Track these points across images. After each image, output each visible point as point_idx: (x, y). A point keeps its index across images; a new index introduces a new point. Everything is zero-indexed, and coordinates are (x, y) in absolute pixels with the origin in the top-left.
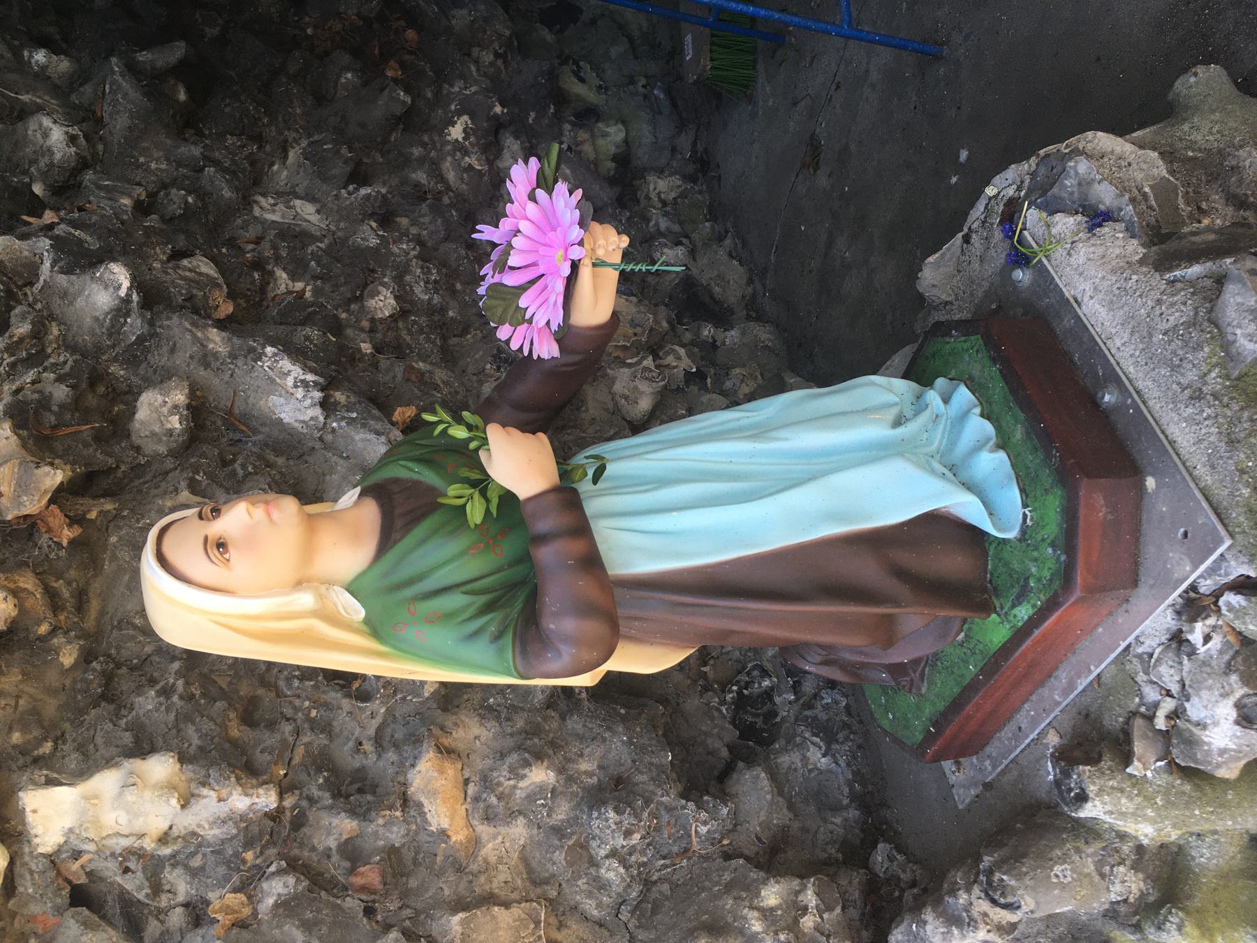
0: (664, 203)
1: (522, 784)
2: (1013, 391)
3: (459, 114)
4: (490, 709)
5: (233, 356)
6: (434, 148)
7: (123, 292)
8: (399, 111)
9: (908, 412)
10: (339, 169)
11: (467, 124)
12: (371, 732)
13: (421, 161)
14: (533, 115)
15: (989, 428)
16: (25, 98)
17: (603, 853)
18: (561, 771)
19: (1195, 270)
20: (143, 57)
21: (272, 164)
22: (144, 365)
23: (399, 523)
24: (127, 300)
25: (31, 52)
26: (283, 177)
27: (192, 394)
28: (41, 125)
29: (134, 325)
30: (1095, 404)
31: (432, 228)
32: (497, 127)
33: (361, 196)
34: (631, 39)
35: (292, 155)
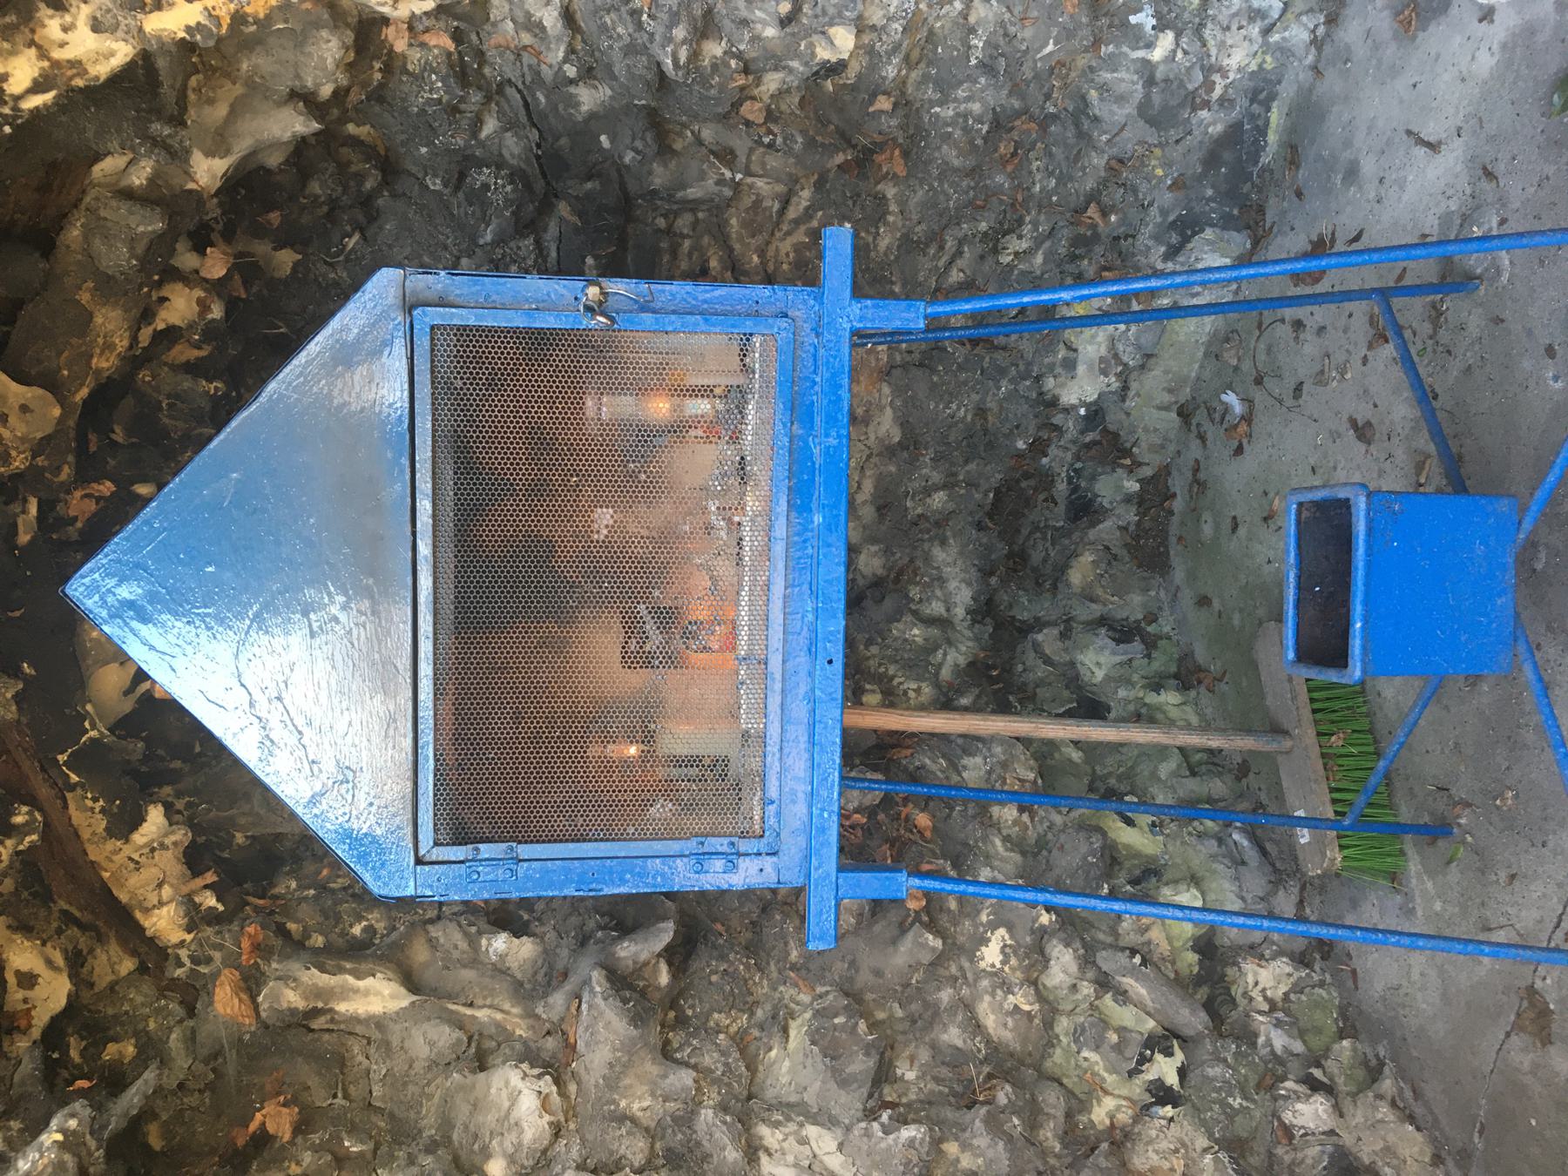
3: (993, 926)
6: (966, 982)
11: (1003, 940)
25: (489, 940)
26: (784, 1070)
28: (507, 1083)
33: (902, 1140)
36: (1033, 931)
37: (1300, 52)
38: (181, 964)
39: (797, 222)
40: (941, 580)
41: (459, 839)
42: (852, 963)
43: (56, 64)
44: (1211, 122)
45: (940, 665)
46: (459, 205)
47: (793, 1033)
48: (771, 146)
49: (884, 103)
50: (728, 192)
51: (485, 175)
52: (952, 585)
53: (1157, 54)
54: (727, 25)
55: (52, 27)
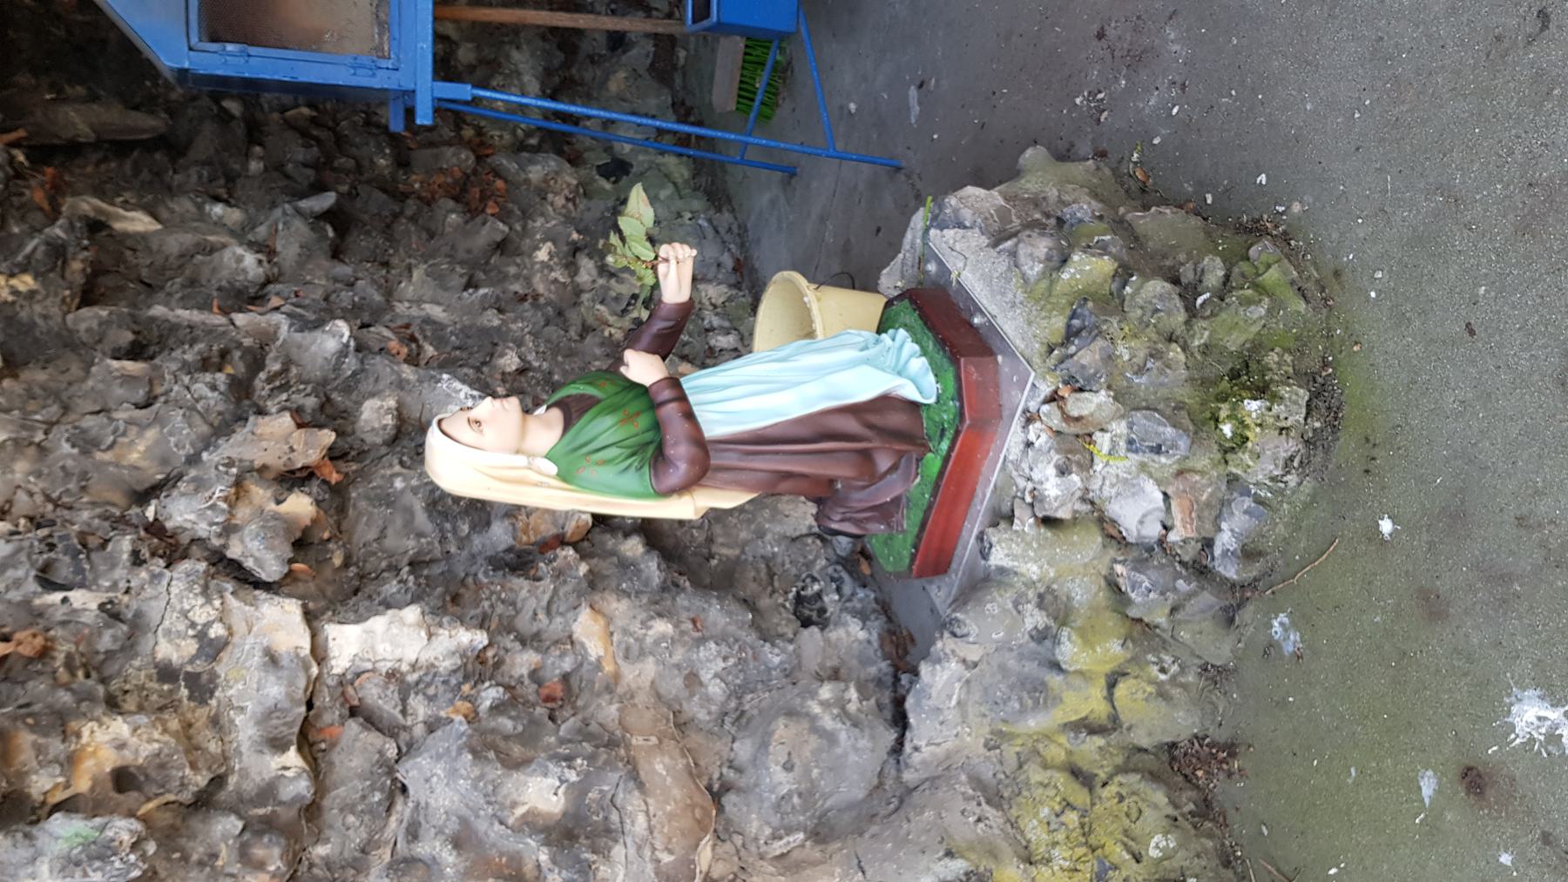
1: (651, 633)
2: (926, 324)
3: (544, 241)
4: (624, 591)
5: (420, 381)
6: (525, 267)
7: (345, 340)
8: (499, 238)
10: (457, 281)
12: (544, 603)
13: (517, 277)
15: (916, 347)
16: (211, 238)
17: (709, 676)
18: (676, 626)
20: (304, 204)
21: (400, 282)
22: (355, 392)
23: (574, 415)
24: (347, 346)
27: (398, 402)
29: (351, 364)
30: (971, 325)
32: (576, 249)
34: (675, 184)
35: (416, 274)
36: (568, 244)
40: (518, 74)
41: (214, 40)
42: (453, 247)
52: (526, 78)
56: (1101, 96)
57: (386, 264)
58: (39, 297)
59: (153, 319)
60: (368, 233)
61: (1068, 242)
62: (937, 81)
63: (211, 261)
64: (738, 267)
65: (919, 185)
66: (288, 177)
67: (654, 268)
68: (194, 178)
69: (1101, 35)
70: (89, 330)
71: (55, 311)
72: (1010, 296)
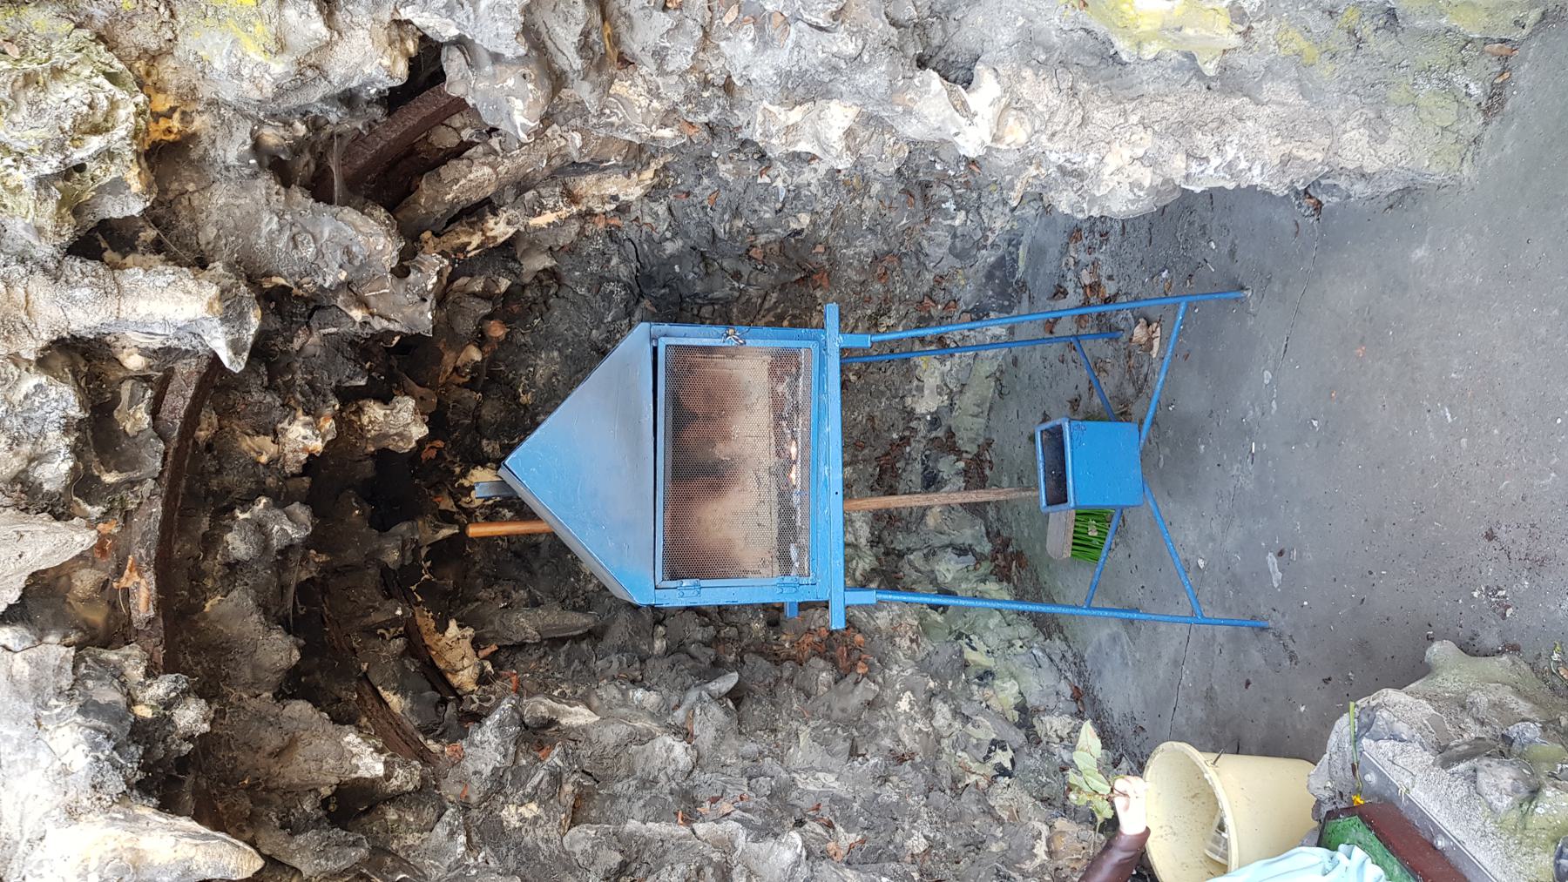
0: (1062, 739)
9: (1329, 866)
10: (842, 746)
13: (886, 731)
14: (950, 683)
19: (1462, 767)
31: (915, 782)
32: (932, 694)
37: (1032, 221)
38: (474, 702)
39: (769, 310)
42: (829, 707)
43: (487, 238)
44: (988, 257)
45: (855, 570)
46: (597, 303)
47: (801, 739)
48: (762, 270)
49: (820, 249)
50: (736, 294)
51: (611, 286)
52: (858, 524)
53: (957, 223)
54: (746, 212)
55: (491, 223)
56: (1501, 593)
57: (774, 731)
58: (541, 822)
59: (631, 835)
60: (759, 702)
61: (1530, 770)
62: (1300, 553)
63: (644, 750)
64: (1077, 696)
65: (1292, 647)
66: (693, 658)
67: (1110, 801)
68: (615, 665)
69: (1490, 536)
70: (584, 852)
71: (554, 834)
72: (1478, 824)
